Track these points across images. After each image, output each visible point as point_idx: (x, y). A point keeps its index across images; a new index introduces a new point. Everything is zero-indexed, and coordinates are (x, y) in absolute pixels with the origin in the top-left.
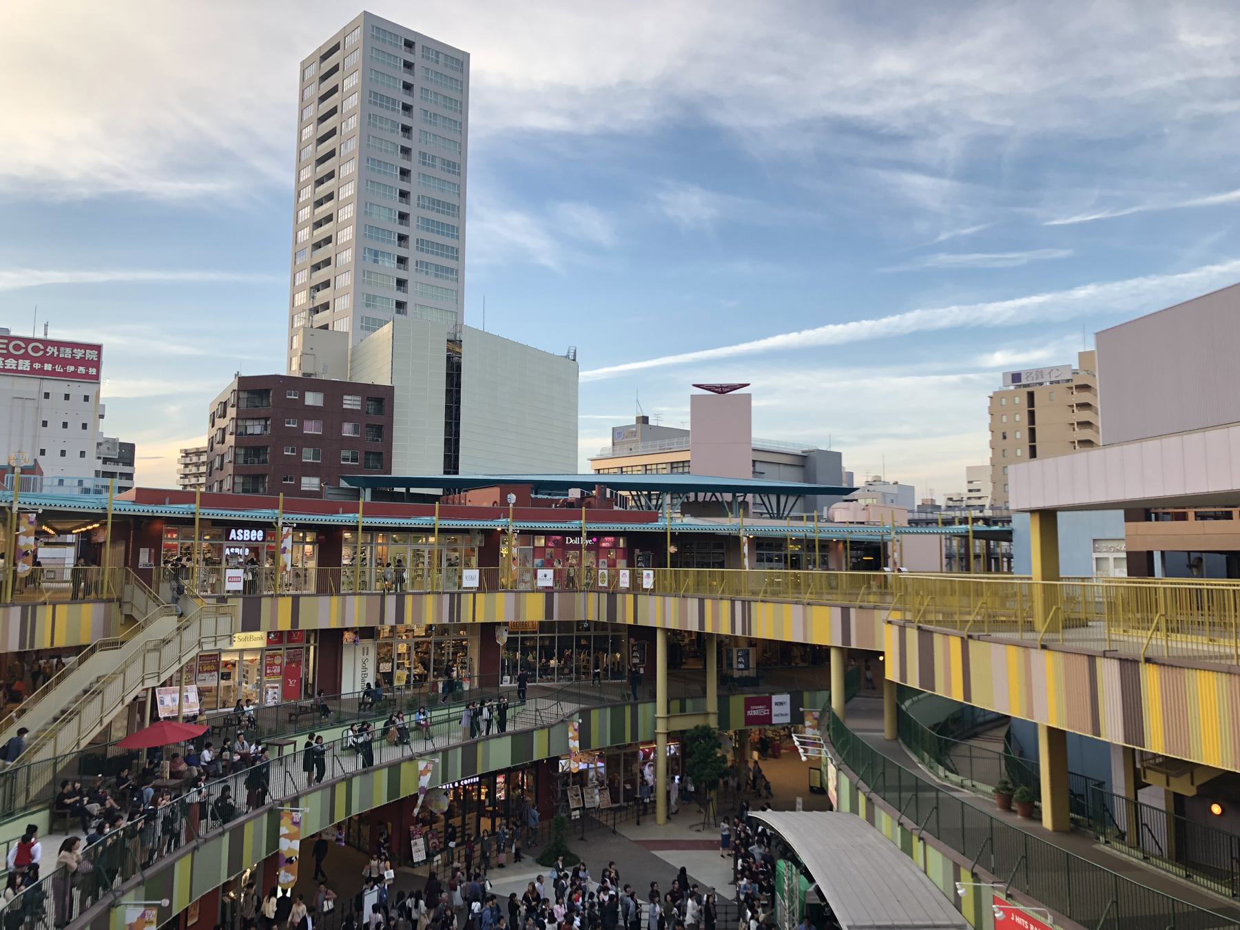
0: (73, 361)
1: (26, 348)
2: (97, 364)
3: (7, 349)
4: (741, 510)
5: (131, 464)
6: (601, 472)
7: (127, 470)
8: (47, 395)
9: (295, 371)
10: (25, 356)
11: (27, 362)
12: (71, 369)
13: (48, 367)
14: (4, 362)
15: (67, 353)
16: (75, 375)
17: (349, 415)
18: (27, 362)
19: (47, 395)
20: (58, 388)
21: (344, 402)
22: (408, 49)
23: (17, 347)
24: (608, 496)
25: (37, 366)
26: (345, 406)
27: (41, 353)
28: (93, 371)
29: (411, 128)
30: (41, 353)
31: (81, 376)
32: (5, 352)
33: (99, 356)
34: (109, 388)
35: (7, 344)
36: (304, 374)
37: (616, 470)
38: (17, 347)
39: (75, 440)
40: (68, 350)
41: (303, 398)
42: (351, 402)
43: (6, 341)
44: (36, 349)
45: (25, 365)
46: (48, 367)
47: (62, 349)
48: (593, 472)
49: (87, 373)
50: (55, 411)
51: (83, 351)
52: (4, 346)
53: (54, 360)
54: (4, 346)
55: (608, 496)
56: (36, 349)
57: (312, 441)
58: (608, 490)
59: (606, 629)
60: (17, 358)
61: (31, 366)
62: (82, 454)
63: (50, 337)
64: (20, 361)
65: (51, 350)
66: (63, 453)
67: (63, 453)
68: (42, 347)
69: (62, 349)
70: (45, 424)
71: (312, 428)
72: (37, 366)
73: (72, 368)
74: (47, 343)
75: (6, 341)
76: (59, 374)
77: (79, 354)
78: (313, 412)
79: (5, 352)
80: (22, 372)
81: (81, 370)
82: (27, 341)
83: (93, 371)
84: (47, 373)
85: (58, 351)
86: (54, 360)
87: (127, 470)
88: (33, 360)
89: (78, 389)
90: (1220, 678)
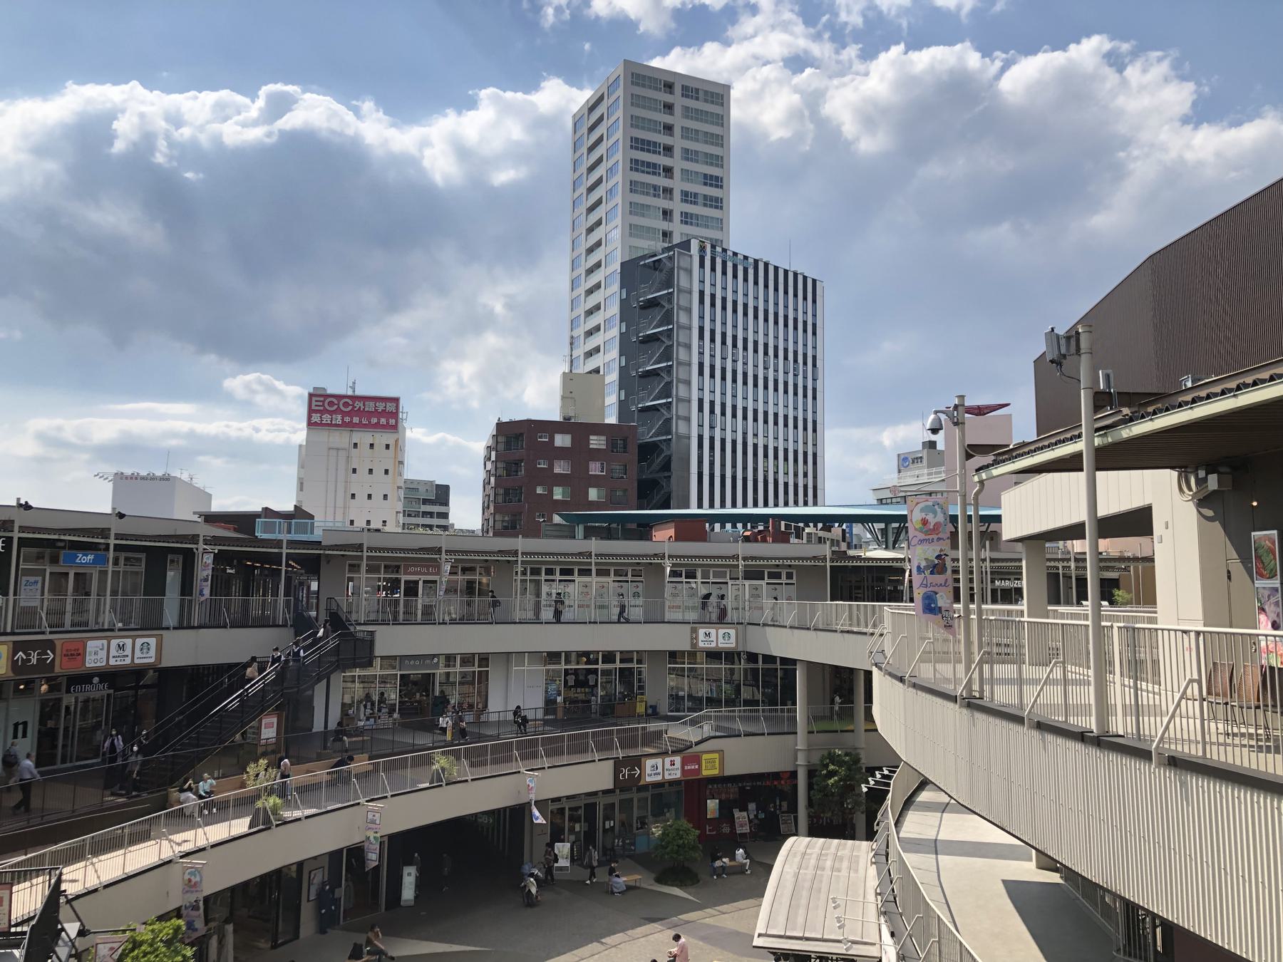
0: (376, 413)
1: (338, 404)
2: (395, 415)
3: (323, 405)
4: (987, 543)
5: (446, 504)
6: (884, 501)
7: (442, 509)
8: (355, 445)
9: (556, 416)
10: (338, 411)
11: (339, 417)
12: (374, 420)
13: (356, 420)
14: (321, 417)
15: (370, 406)
16: (377, 425)
17: (595, 454)
18: (339, 417)
19: (355, 445)
20: (364, 438)
21: (591, 442)
22: (668, 89)
23: (331, 404)
24: (783, 528)
25: (347, 419)
26: (591, 446)
27: (350, 408)
28: (392, 422)
29: (673, 168)
30: (350, 408)
31: (384, 427)
32: (322, 408)
33: (309, 417)
34: (415, 433)
35: (323, 402)
36: (565, 419)
37: (899, 500)
38: (331, 404)
39: (381, 484)
40: (372, 404)
41: (552, 439)
42: (597, 442)
43: (322, 399)
44: (346, 404)
45: (338, 419)
46: (356, 420)
47: (367, 403)
48: (875, 502)
49: (388, 423)
50: (362, 459)
51: (384, 404)
52: (321, 404)
53: (360, 413)
54: (321, 404)
55: (783, 528)
56: (346, 404)
57: (561, 480)
58: (783, 523)
59: (631, 660)
60: (331, 413)
61: (343, 420)
62: (385, 497)
63: (358, 393)
64: (334, 416)
65: (358, 404)
66: (370, 496)
67: (370, 496)
68: (350, 402)
69: (367, 403)
70: (354, 471)
71: (560, 468)
72: (347, 419)
73: (374, 420)
74: (354, 398)
75: (322, 399)
76: (365, 426)
77: (381, 406)
78: (562, 453)
79: (322, 408)
80: (336, 425)
81: (383, 421)
82: (339, 397)
83: (392, 422)
84: (355, 425)
85: (364, 405)
86: (360, 413)
87: (442, 509)
88: (344, 414)
89: (382, 438)
90: (1115, 730)
